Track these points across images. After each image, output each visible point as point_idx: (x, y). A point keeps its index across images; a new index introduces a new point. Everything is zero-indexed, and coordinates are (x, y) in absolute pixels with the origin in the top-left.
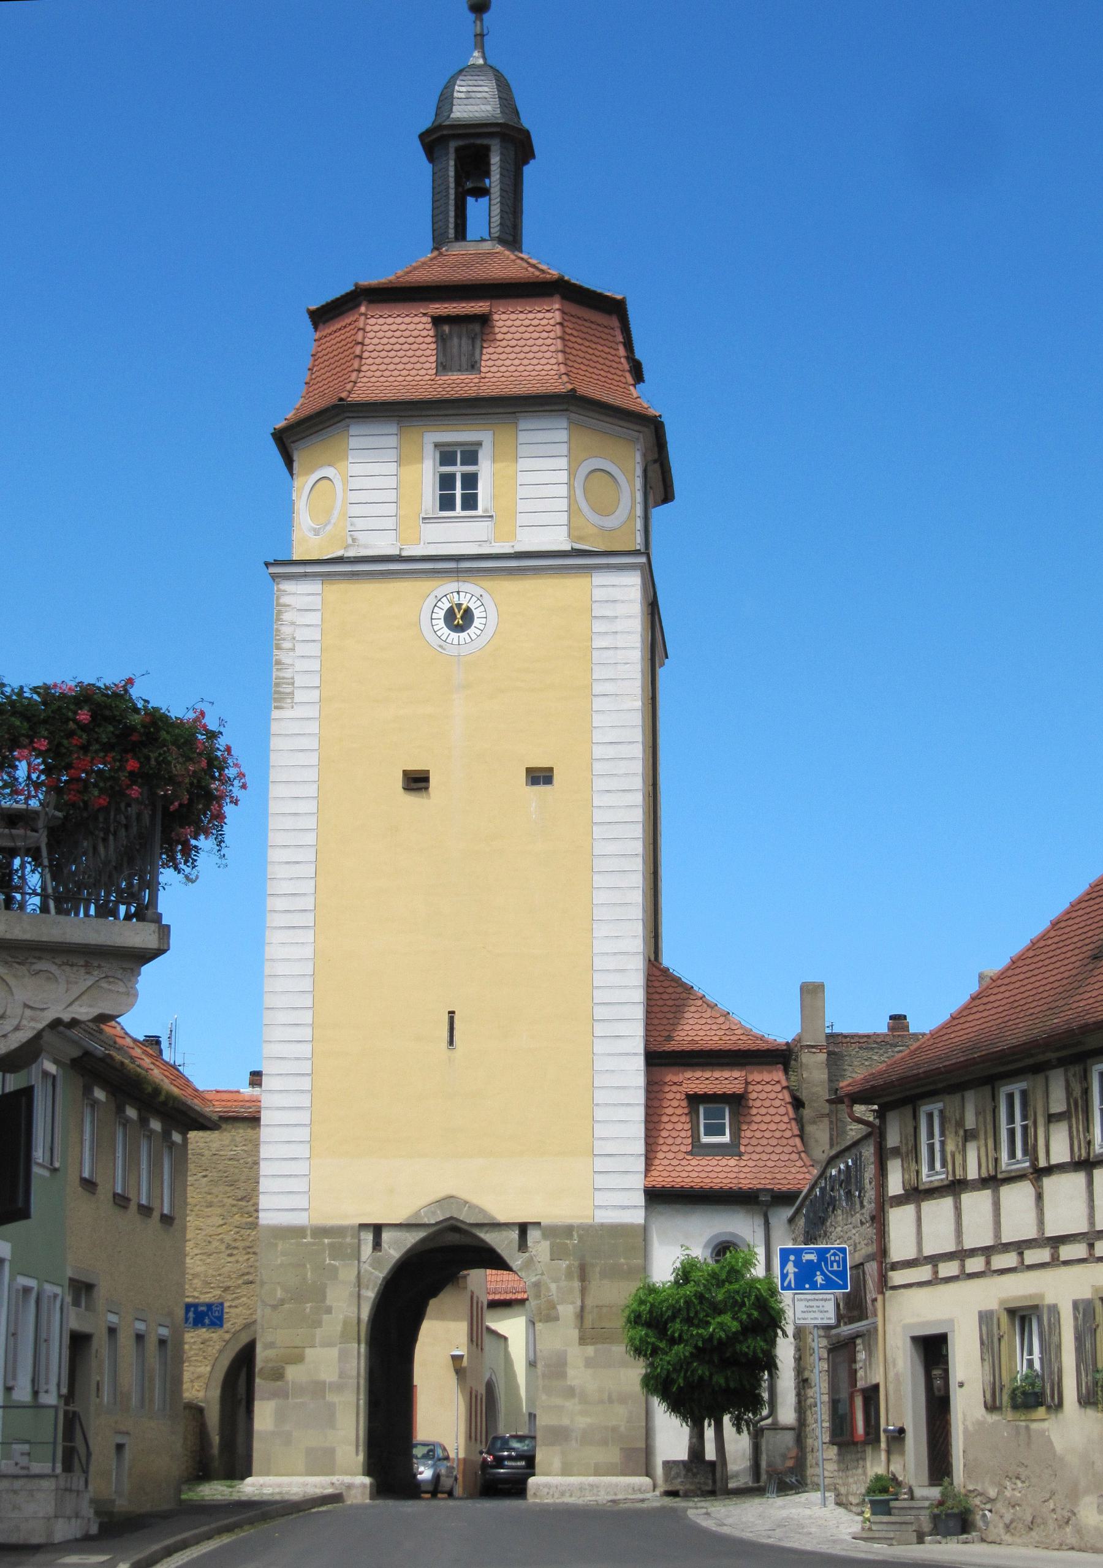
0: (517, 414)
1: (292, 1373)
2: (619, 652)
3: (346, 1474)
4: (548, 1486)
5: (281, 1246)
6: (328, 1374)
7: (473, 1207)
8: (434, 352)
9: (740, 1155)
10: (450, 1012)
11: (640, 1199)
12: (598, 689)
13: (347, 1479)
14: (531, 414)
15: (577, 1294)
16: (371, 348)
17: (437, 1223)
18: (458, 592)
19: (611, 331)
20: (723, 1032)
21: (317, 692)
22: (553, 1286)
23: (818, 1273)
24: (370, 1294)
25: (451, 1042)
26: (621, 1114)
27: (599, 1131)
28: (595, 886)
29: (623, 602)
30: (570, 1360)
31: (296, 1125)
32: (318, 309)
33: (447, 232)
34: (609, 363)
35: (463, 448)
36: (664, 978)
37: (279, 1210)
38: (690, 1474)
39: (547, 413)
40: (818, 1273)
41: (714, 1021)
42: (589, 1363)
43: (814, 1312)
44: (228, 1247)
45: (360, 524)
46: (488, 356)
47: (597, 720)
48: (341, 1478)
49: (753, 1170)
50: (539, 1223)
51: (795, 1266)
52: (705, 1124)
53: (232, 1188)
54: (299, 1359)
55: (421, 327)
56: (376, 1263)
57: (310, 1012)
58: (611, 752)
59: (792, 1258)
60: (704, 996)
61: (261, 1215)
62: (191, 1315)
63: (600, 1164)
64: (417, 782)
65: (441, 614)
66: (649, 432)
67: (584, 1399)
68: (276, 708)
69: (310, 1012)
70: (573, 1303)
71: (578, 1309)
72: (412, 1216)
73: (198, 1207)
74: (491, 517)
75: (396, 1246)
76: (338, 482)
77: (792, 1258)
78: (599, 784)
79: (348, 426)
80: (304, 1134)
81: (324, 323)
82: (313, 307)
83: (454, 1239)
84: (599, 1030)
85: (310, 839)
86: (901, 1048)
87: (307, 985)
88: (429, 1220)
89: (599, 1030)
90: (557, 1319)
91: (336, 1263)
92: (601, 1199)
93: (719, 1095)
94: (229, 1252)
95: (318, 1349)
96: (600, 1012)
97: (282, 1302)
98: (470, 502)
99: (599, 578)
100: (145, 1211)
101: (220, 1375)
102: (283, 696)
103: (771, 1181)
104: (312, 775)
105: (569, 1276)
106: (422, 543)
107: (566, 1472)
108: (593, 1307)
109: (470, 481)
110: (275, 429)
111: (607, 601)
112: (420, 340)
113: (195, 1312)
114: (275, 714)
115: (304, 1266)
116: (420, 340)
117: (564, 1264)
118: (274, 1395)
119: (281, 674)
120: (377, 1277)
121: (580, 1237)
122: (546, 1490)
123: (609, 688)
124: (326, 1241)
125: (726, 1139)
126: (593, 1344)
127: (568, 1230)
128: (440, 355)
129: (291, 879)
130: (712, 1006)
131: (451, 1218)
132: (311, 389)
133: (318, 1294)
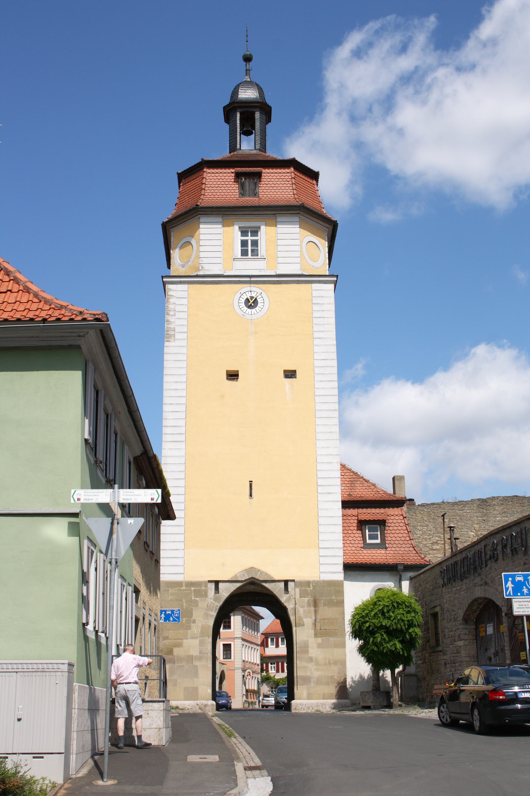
0: (276, 215)
1: (177, 651)
2: (325, 319)
3: (204, 700)
4: (301, 704)
6: (195, 652)
7: (262, 572)
8: (238, 188)
9: (386, 548)
10: (250, 481)
11: (341, 568)
12: (316, 335)
13: (205, 702)
14: (283, 215)
15: (313, 614)
16: (209, 186)
17: (245, 580)
18: (251, 291)
19: (313, 185)
20: (374, 493)
21: (186, 334)
23: (524, 587)
27: (321, 537)
28: (316, 424)
29: (326, 297)
30: (310, 645)
31: (177, 534)
32: (182, 172)
33: (236, 146)
34: (314, 198)
35: (251, 229)
36: (344, 469)
38: (376, 698)
39: (290, 215)
40: (524, 587)
41: (369, 488)
42: (319, 646)
43: (523, 608)
47: (316, 349)
48: (201, 701)
49: (393, 555)
51: (512, 584)
52: (369, 534)
54: (179, 645)
56: (216, 599)
57: (184, 481)
58: (323, 363)
59: (510, 579)
60: (363, 477)
62: (163, 616)
63: (322, 552)
64: (233, 376)
65: (243, 301)
66: (331, 228)
67: (317, 663)
68: (167, 341)
69: (184, 481)
70: (311, 617)
71: (314, 620)
72: (234, 577)
74: (265, 259)
75: (226, 590)
77: (510, 579)
78: (317, 378)
79: (199, 218)
80: (181, 538)
81: (185, 178)
82: (179, 172)
83: (252, 588)
84: (320, 490)
85: (183, 401)
86: (436, 506)
87: (182, 468)
88: (241, 579)
89: (320, 490)
90: (303, 625)
91: (197, 599)
92: (323, 568)
93: (376, 520)
95: (189, 640)
96: (320, 482)
98: (255, 253)
99: (315, 286)
102: (170, 336)
103: (402, 560)
104: (184, 371)
105: (309, 605)
106: (233, 269)
107: (309, 697)
108: (320, 619)
109: (255, 243)
110: (163, 222)
111: (319, 297)
113: (165, 614)
114: (166, 344)
115: (182, 600)
117: (306, 599)
119: (169, 326)
120: (217, 606)
121: (314, 586)
122: (300, 707)
124: (192, 588)
125: (378, 541)
126: (320, 637)
127: (308, 583)
129: (174, 419)
130: (367, 481)
131: (252, 578)
132: (180, 201)
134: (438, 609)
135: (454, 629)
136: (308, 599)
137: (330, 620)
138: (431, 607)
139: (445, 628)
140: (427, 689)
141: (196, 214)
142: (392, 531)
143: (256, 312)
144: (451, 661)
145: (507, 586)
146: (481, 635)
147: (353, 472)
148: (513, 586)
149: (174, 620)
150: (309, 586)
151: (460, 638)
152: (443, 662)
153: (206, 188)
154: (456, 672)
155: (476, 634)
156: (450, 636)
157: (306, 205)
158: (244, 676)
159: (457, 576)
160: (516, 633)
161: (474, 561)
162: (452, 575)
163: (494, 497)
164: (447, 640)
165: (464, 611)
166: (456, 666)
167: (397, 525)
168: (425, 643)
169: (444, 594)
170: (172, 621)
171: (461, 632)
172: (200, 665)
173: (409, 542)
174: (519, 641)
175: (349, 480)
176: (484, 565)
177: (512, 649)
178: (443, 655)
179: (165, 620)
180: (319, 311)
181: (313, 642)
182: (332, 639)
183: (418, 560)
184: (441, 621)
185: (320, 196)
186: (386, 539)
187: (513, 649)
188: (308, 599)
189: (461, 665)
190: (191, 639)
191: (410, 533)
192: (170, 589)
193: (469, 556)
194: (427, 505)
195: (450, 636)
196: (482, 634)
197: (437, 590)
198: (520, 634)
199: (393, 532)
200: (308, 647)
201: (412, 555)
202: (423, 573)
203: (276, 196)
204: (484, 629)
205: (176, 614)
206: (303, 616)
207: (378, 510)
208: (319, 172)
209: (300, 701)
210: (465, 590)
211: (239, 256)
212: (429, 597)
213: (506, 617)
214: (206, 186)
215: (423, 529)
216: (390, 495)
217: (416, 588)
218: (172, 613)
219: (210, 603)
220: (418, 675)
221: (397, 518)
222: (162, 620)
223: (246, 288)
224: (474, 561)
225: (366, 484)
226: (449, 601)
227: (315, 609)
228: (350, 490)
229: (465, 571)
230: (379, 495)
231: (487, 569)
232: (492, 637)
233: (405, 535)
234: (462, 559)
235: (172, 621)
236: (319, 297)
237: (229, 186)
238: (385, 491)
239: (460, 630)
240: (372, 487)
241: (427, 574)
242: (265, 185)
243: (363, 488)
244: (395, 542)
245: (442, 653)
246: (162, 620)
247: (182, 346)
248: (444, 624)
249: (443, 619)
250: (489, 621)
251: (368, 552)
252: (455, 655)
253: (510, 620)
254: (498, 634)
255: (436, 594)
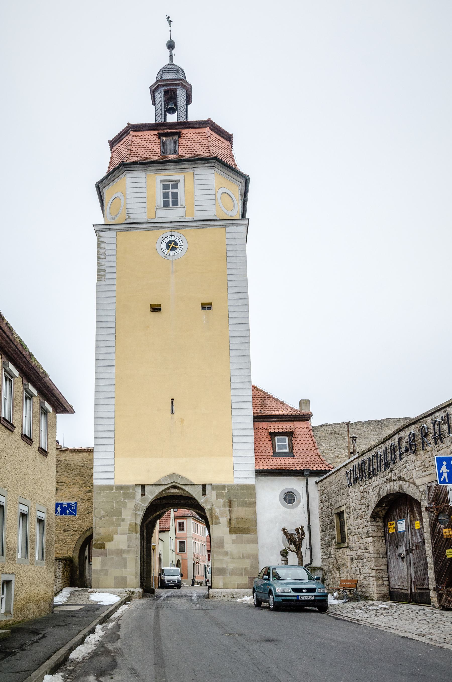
1: (109, 546)
2: (238, 258)
3: (132, 588)
5: (103, 494)
6: (123, 546)
10: (171, 399)
13: (132, 590)
16: (134, 147)
18: (172, 236)
21: (115, 274)
22: (217, 510)
24: (141, 513)
25: (172, 411)
26: (244, 439)
29: (239, 239)
30: (225, 540)
37: (101, 479)
42: (234, 542)
44: (81, 499)
45: (131, 211)
46: (181, 149)
48: (129, 589)
50: (211, 484)
53: (83, 477)
54: (111, 540)
55: (154, 139)
56: (142, 501)
57: (113, 400)
58: (236, 296)
61: (94, 481)
62: (59, 509)
63: (236, 460)
64: (156, 309)
66: (243, 181)
67: (232, 557)
70: (226, 517)
71: (229, 519)
73: (69, 485)
74: (184, 207)
75: (150, 495)
76: (122, 198)
77: (445, 463)
89: (234, 406)
90: (219, 523)
92: (237, 474)
94: (82, 501)
95: (119, 536)
97: (103, 516)
98: (175, 203)
99: (229, 229)
100: (28, 440)
101: (78, 548)
105: (224, 505)
106: (156, 218)
107: (225, 587)
109: (175, 195)
111: (232, 238)
112: (154, 144)
113: (61, 507)
115: (113, 502)
116: (154, 144)
117: (222, 501)
118: (101, 555)
120: (143, 506)
123: (234, 272)
124: (121, 491)
125: (287, 451)
126: (234, 534)
128: (162, 149)
129: (105, 347)
130: (276, 400)
133: (118, 513)
134: (344, 508)
135: (361, 526)
136: (223, 500)
137: (243, 519)
138: (336, 507)
139: (352, 526)
140: (332, 581)
141: (123, 171)
142: (299, 442)
143: (176, 254)
144: (358, 557)
145: (441, 472)
146: (390, 532)
147: (263, 392)
148: (448, 471)
149: (71, 513)
150: (224, 489)
151: (368, 535)
152: (349, 558)
153: (132, 149)
154: (363, 568)
155: (384, 531)
156: (357, 533)
157: (212, 121)
158: (194, 563)
159: (365, 474)
160: (440, 528)
161: (386, 457)
162: (360, 475)
163: (389, 419)
164: (353, 537)
165: (373, 508)
166: (363, 561)
167: (304, 436)
168: (330, 540)
169: (350, 494)
170: (68, 514)
171: (369, 529)
172: (128, 558)
173: (315, 451)
174: (445, 537)
175: (260, 399)
176: (398, 459)
177: (435, 545)
178: (349, 551)
179: (61, 513)
180: (232, 251)
181: (228, 538)
182: (245, 535)
183: (323, 467)
184: (347, 519)
185: (233, 156)
186: (294, 448)
187: (436, 546)
188: (223, 500)
189: (369, 561)
190: (120, 535)
191: (315, 443)
192: (102, 492)
193: (379, 453)
194: (330, 425)
195: (357, 533)
196: (392, 531)
197: (342, 490)
198: (445, 530)
199: (300, 442)
200: (223, 542)
201: (317, 462)
202: (329, 476)
203: (194, 152)
204: (394, 526)
205: (73, 507)
206: (219, 515)
207: (286, 424)
208: (232, 134)
209: (216, 589)
210: (374, 488)
211: (162, 206)
212: (334, 498)
213: (427, 512)
214: (132, 147)
215: (326, 445)
216: (297, 411)
217: (322, 491)
218: (68, 506)
219: (137, 504)
220: (324, 568)
221: (303, 430)
222: (58, 513)
223: (167, 233)
224: (386, 457)
225: (276, 402)
226: (356, 500)
227: (230, 510)
228: (261, 408)
229: (375, 468)
230: (287, 411)
231: (402, 463)
232: (403, 534)
233: (311, 445)
234: (371, 458)
235: (68, 514)
236: (232, 238)
237: (152, 146)
238: (292, 408)
239: (369, 527)
240: (281, 405)
241: (334, 476)
242: (184, 144)
243: (272, 405)
244: (302, 451)
245: (348, 549)
246: (58, 513)
247: (111, 285)
248: (349, 522)
249: (349, 517)
250: (400, 518)
251: (277, 460)
252: (362, 551)
253: (432, 515)
254: (413, 531)
255: (341, 494)
